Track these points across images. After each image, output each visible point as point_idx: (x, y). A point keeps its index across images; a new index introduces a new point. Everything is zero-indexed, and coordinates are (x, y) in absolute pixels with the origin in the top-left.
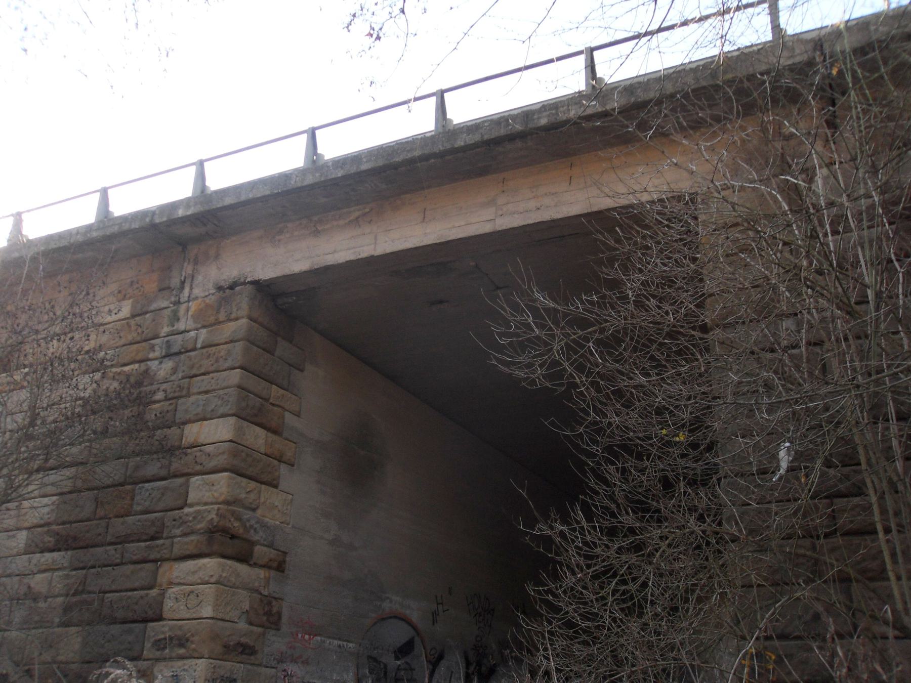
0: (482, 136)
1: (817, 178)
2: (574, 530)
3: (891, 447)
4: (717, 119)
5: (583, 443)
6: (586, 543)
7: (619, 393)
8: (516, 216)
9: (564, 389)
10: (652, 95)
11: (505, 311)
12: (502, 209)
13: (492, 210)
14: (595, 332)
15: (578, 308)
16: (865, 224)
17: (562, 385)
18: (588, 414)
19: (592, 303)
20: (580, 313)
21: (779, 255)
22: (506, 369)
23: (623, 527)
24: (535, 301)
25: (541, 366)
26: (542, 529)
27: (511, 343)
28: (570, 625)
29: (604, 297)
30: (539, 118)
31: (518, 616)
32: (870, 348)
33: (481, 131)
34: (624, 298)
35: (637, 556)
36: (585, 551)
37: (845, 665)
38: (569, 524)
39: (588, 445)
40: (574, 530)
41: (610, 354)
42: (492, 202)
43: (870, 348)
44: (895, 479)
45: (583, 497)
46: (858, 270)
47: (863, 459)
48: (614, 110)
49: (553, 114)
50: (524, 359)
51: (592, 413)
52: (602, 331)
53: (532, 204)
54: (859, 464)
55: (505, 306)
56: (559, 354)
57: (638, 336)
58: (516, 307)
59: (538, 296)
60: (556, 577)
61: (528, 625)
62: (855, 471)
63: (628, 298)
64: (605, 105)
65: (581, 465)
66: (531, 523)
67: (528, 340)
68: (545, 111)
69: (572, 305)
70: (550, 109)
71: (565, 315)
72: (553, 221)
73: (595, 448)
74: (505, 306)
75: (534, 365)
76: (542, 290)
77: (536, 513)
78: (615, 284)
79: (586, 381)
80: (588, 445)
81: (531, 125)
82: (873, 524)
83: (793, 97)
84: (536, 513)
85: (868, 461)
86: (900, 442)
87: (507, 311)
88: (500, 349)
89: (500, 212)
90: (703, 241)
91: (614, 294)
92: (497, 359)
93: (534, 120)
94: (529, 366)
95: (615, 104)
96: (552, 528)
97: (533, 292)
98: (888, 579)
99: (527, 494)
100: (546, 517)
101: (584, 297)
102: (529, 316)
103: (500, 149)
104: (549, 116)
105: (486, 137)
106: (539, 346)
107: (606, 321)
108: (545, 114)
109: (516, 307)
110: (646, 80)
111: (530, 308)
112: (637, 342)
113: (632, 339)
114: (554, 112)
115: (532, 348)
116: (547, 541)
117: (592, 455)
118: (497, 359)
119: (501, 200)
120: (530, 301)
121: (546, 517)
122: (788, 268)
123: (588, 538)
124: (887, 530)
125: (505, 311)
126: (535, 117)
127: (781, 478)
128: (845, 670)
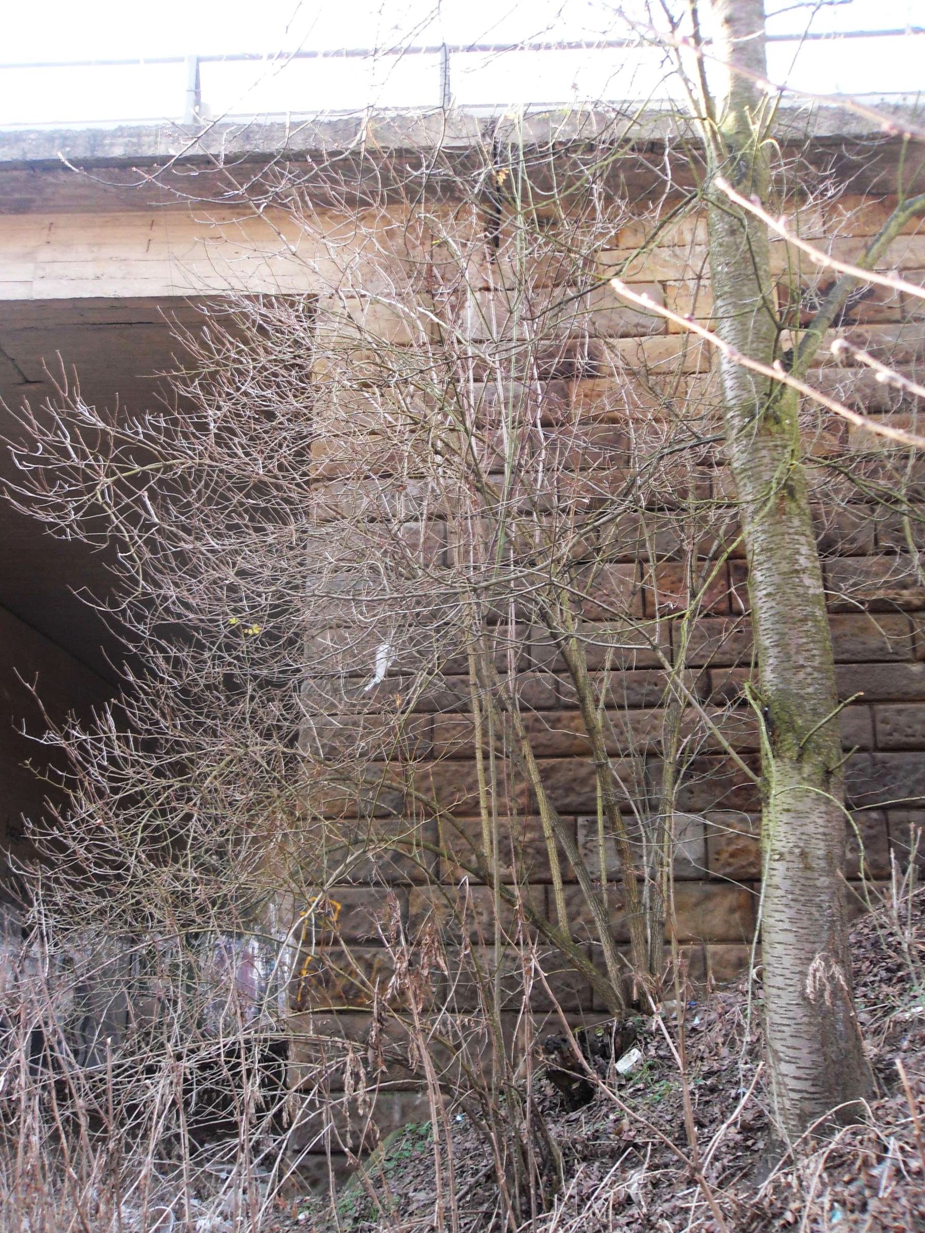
0: (25, 153)
1: (467, 304)
2: (99, 740)
3: (505, 656)
4: (351, 201)
5: (125, 619)
6: (112, 760)
7: (182, 557)
8: (64, 282)
9: (105, 546)
10: (276, 146)
11: (31, 426)
12: (44, 269)
13: (31, 266)
14: (157, 470)
15: (137, 433)
16: (513, 374)
17: (102, 539)
18: (137, 583)
19: (157, 429)
20: (140, 441)
21: (408, 400)
22: (25, 509)
23: (167, 741)
24: (74, 416)
25: (77, 510)
26: (51, 738)
27: (34, 472)
28: (78, 869)
29: (175, 422)
30: (112, 145)
31: (6, 856)
32: (496, 541)
33: (24, 145)
34: (203, 427)
35: (181, 781)
36: (112, 772)
37: (407, 958)
38: (93, 733)
39: (131, 622)
40: (99, 740)
41: (175, 501)
42: (28, 256)
43: (496, 541)
44: (505, 696)
45: (116, 702)
46: (499, 432)
47: (472, 670)
48: (217, 157)
49: (134, 144)
50: (52, 496)
51: (142, 582)
52: (168, 469)
53: (90, 270)
54: (467, 673)
55: (32, 417)
56: (103, 497)
57: (217, 483)
58: (47, 421)
59: (82, 408)
60: (66, 806)
61: (19, 868)
62: (463, 682)
63: (208, 430)
64: (208, 147)
65: (118, 653)
66: (38, 728)
67: (62, 469)
68: (122, 136)
69: (130, 429)
70: (131, 136)
71: (118, 442)
72: (117, 299)
73: (141, 628)
74: (32, 417)
75: (65, 507)
76: (88, 401)
77: (46, 717)
78: (190, 406)
79: (140, 537)
80: (131, 622)
81: (100, 154)
82: (473, 747)
83: (450, 191)
84: (46, 717)
85: (478, 671)
86: (516, 653)
87: (34, 427)
88: (19, 477)
89: (41, 273)
90: (316, 370)
91: (191, 418)
92: (13, 493)
93: (104, 146)
94: (58, 507)
95: (222, 148)
96: (67, 737)
97: (75, 402)
98: (479, 814)
99: (36, 690)
100: (60, 724)
101: (147, 417)
102: (65, 437)
103: (50, 179)
104: (127, 145)
105: (30, 157)
106: (77, 480)
107: (175, 458)
108: (121, 140)
109: (47, 421)
110: (268, 123)
111: (69, 426)
112: (214, 491)
113: (207, 486)
114: (135, 140)
115: (66, 481)
116: (60, 756)
117: (135, 638)
118: (13, 493)
119: (45, 254)
120: (69, 415)
121: (60, 724)
122: (376, 527)
123: (117, 752)
124: (486, 757)
125: (31, 426)
126: (107, 142)
127: (376, 686)
128: (405, 964)
